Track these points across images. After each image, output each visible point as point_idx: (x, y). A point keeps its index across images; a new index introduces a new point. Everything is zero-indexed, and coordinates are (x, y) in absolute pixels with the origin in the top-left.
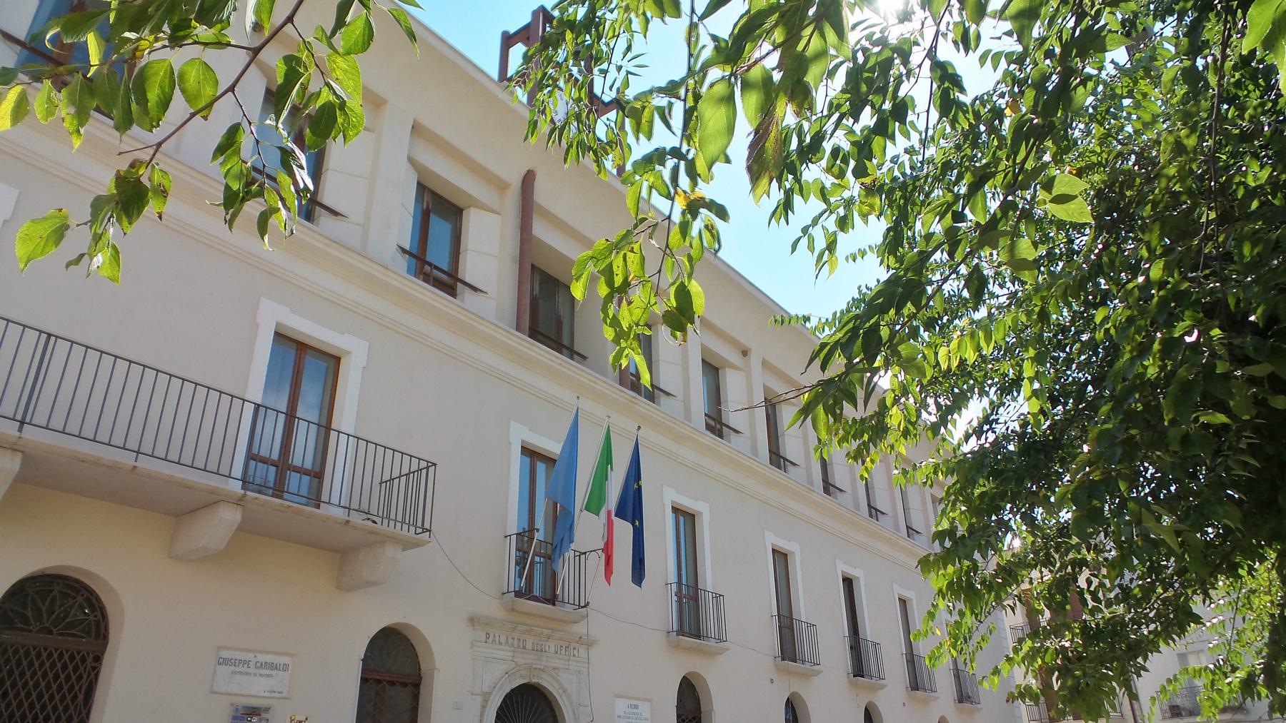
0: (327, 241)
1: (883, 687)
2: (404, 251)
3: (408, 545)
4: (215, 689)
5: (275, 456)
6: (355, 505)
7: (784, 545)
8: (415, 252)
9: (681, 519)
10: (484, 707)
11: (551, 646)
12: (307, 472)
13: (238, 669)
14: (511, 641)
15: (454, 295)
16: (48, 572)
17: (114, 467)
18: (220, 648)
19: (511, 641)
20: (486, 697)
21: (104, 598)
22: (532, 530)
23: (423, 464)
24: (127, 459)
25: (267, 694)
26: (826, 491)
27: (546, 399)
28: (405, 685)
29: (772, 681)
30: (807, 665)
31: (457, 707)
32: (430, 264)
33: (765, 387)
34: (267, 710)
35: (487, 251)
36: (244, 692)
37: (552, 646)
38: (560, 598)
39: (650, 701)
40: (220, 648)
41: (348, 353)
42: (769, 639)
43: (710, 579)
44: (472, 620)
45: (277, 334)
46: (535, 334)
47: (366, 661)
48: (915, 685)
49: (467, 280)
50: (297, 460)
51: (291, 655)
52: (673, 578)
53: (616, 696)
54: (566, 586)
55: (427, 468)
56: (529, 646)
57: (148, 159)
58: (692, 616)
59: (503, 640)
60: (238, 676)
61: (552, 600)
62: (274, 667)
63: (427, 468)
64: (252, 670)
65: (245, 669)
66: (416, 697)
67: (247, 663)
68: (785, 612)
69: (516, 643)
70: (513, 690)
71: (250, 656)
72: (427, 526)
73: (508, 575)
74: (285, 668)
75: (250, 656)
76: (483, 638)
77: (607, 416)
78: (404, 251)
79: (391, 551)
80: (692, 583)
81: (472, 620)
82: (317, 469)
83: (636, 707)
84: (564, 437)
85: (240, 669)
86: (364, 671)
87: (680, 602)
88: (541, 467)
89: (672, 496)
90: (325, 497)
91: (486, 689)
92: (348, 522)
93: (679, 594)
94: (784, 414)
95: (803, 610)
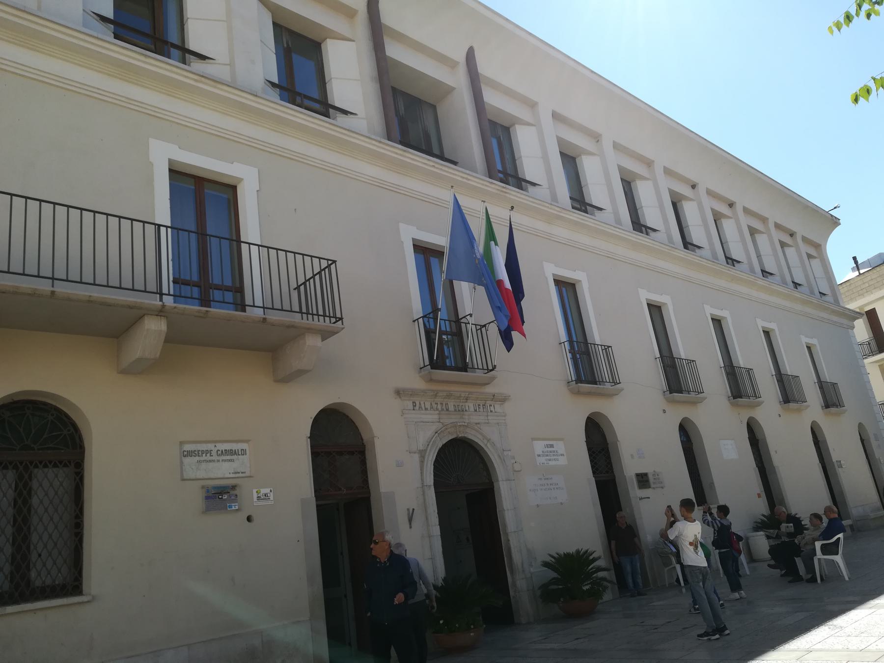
0: (196, 77)
1: (759, 404)
2: (273, 85)
3: (326, 335)
4: (185, 477)
5: (195, 278)
7: (657, 298)
8: (284, 85)
9: (564, 289)
10: (422, 462)
11: (470, 405)
12: (228, 289)
13: (201, 459)
14: (435, 406)
15: (328, 116)
16: (16, 399)
17: (34, 294)
18: (182, 443)
19: (435, 406)
20: (422, 454)
22: (435, 310)
23: (324, 264)
24: (45, 286)
25: (232, 475)
26: (686, 247)
27: (424, 198)
28: (352, 453)
29: (664, 411)
30: (693, 394)
31: (399, 464)
32: (300, 94)
34: (234, 487)
35: (348, 72)
36: (212, 476)
37: (471, 405)
38: (470, 366)
39: (183, 480)
40: (182, 443)
41: (240, 180)
42: (656, 377)
43: (597, 334)
44: (398, 393)
45: (170, 170)
46: (406, 143)
47: (313, 437)
48: (787, 398)
49: (337, 105)
50: (216, 280)
51: (247, 441)
52: (564, 337)
53: (533, 439)
55: (329, 266)
56: (451, 408)
57: (228, 241)
58: (587, 365)
59: (428, 405)
60: (204, 465)
61: (464, 367)
62: (232, 452)
63: (329, 266)
64: (215, 457)
65: (208, 458)
66: (364, 462)
67: (209, 452)
68: (666, 353)
69: (439, 407)
70: (444, 446)
71: (210, 446)
72: (338, 315)
73: (421, 353)
74: (244, 452)
75: (210, 446)
76: (410, 406)
77: (486, 203)
78: (273, 85)
79: (312, 341)
80: (581, 339)
81: (398, 393)
82: (238, 285)
83: (552, 446)
85: (204, 458)
86: (312, 447)
87: (574, 358)
89: (551, 270)
91: (421, 448)
92: (265, 319)
93: (572, 350)
94: (639, 187)
95: (682, 349)
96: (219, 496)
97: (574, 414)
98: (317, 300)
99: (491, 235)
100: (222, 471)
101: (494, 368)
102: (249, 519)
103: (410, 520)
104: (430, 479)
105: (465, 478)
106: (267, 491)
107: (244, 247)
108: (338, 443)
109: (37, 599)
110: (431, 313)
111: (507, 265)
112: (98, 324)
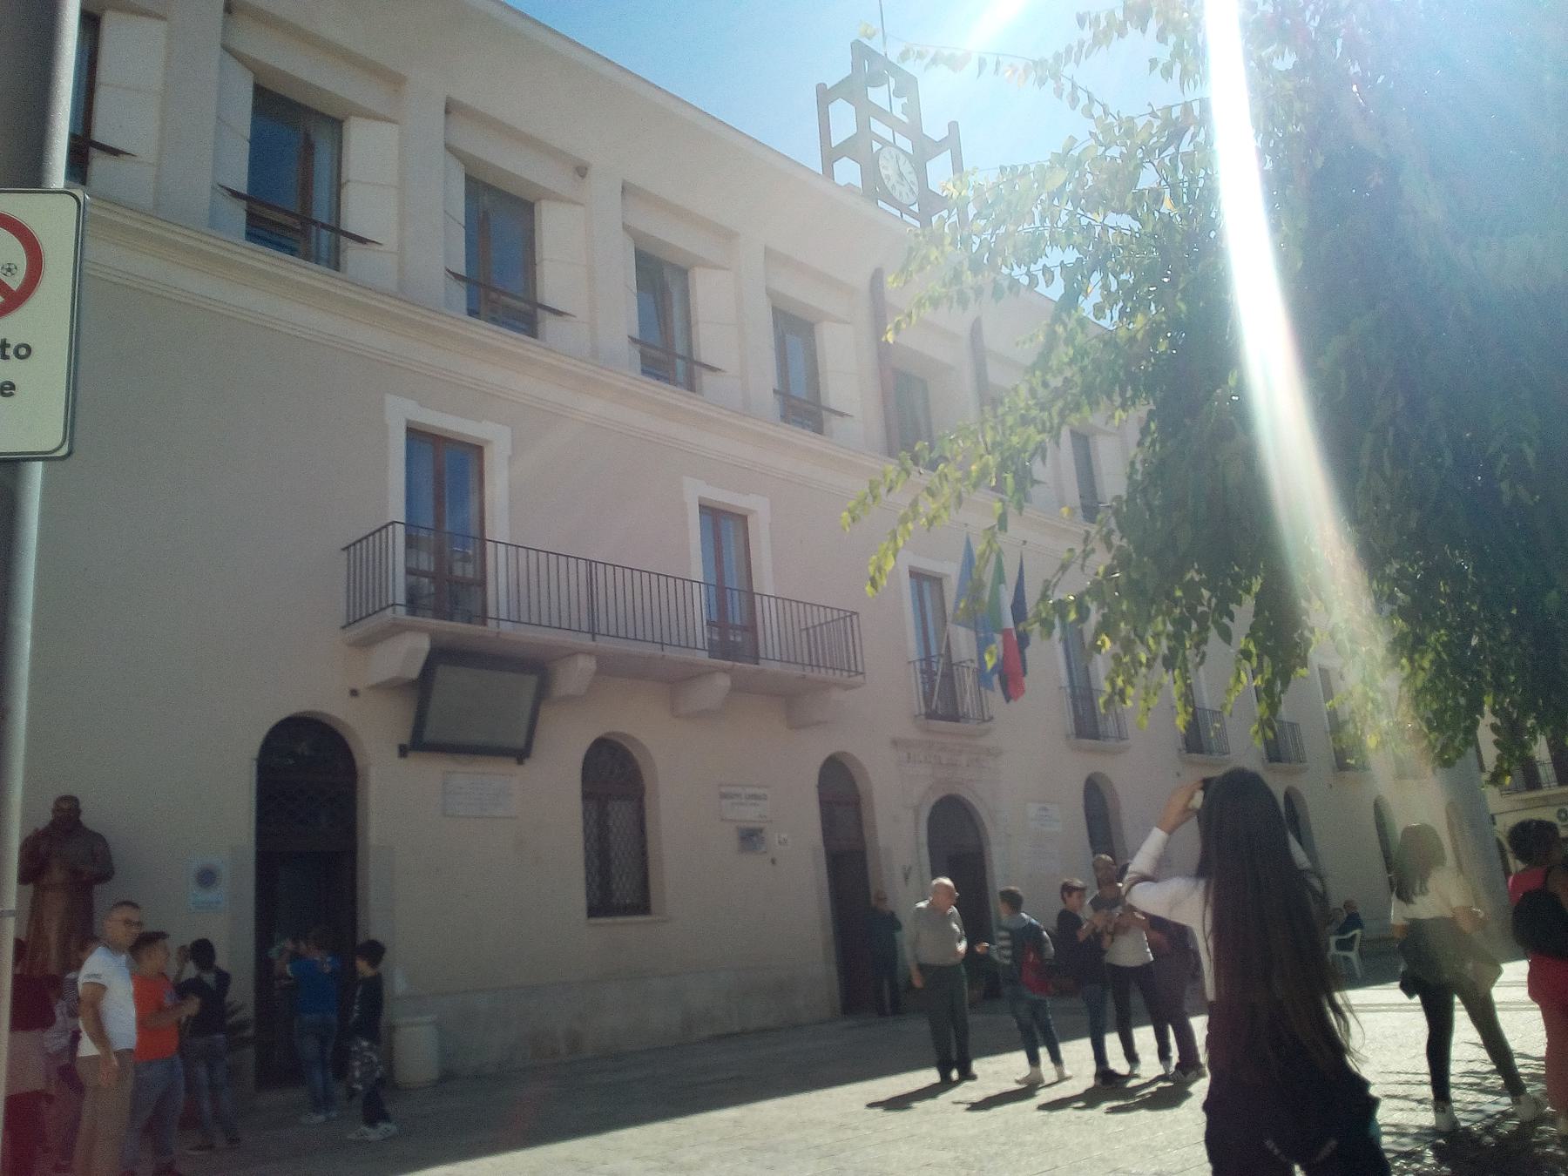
2: (457, 276)
3: (848, 687)
6: (666, 640)
21: (352, 745)
24: (796, 671)
32: (495, 290)
33: (770, 293)
34: (761, 830)
41: (487, 442)
52: (1065, 682)
54: (968, 702)
62: (755, 797)
67: (738, 795)
74: (764, 797)
84: (961, 557)
86: (820, 794)
88: (926, 585)
90: (762, 654)
93: (1073, 696)
96: (750, 838)
97: (1074, 769)
98: (832, 651)
99: (1000, 577)
100: (750, 814)
101: (991, 718)
102: (773, 861)
103: (906, 877)
104: (924, 838)
105: (957, 838)
106: (784, 836)
107: (757, 598)
108: (840, 794)
109: (629, 914)
110: (927, 659)
111: (1013, 607)
112: (675, 681)
